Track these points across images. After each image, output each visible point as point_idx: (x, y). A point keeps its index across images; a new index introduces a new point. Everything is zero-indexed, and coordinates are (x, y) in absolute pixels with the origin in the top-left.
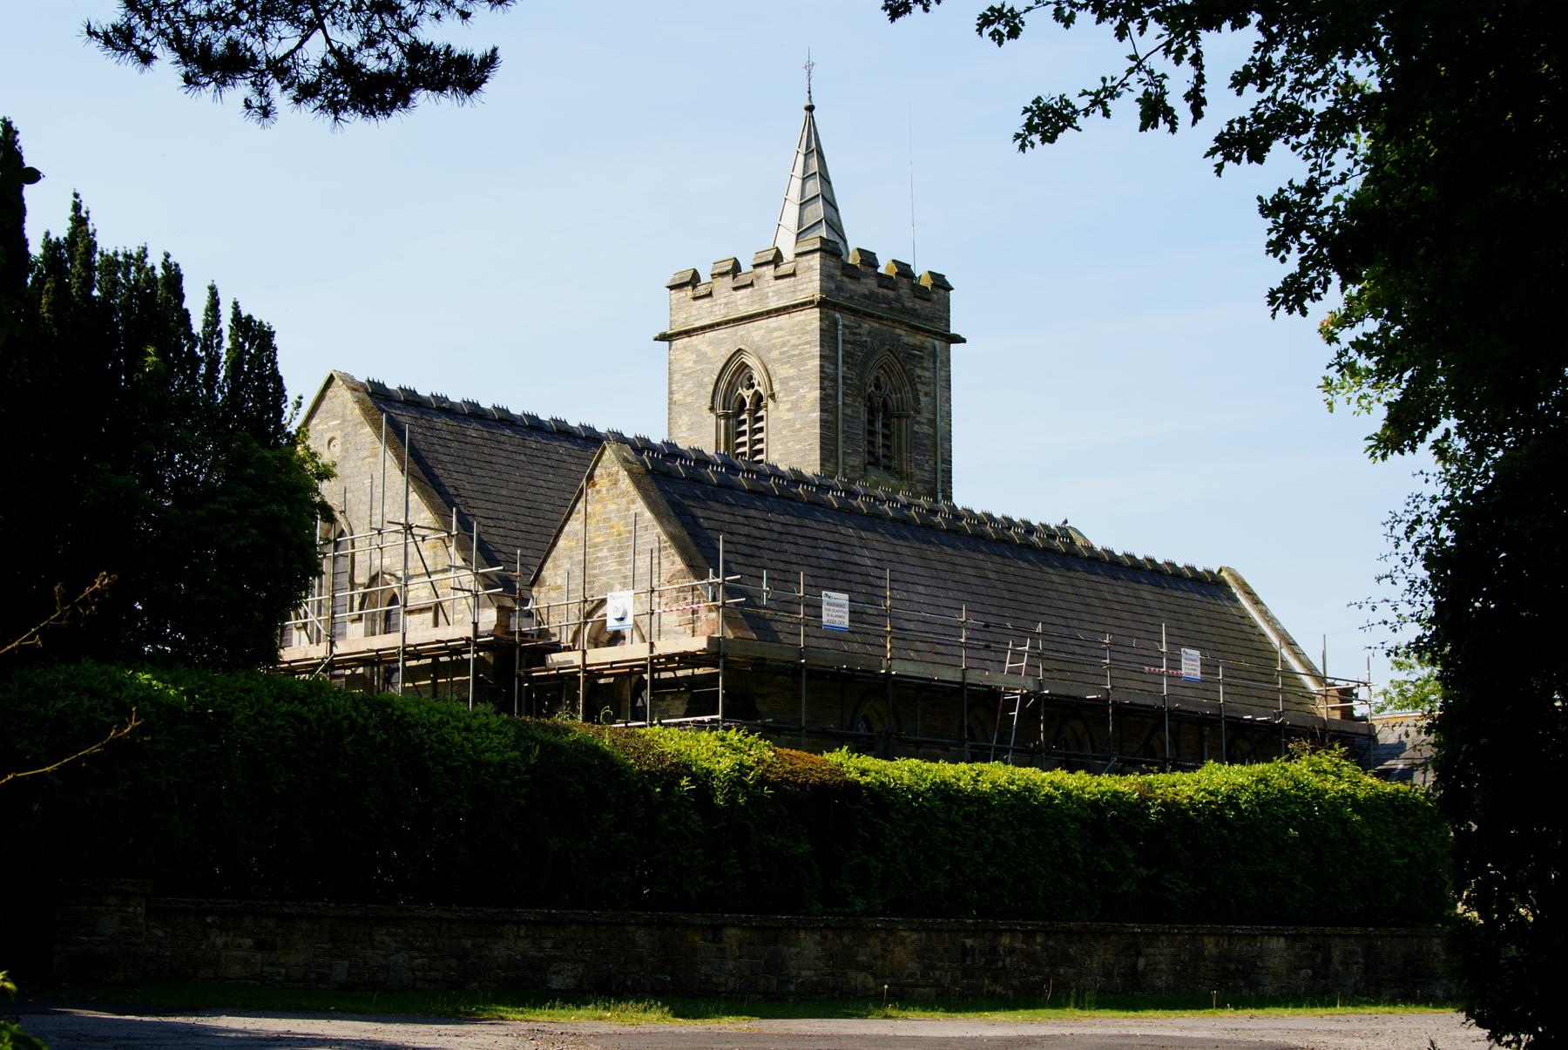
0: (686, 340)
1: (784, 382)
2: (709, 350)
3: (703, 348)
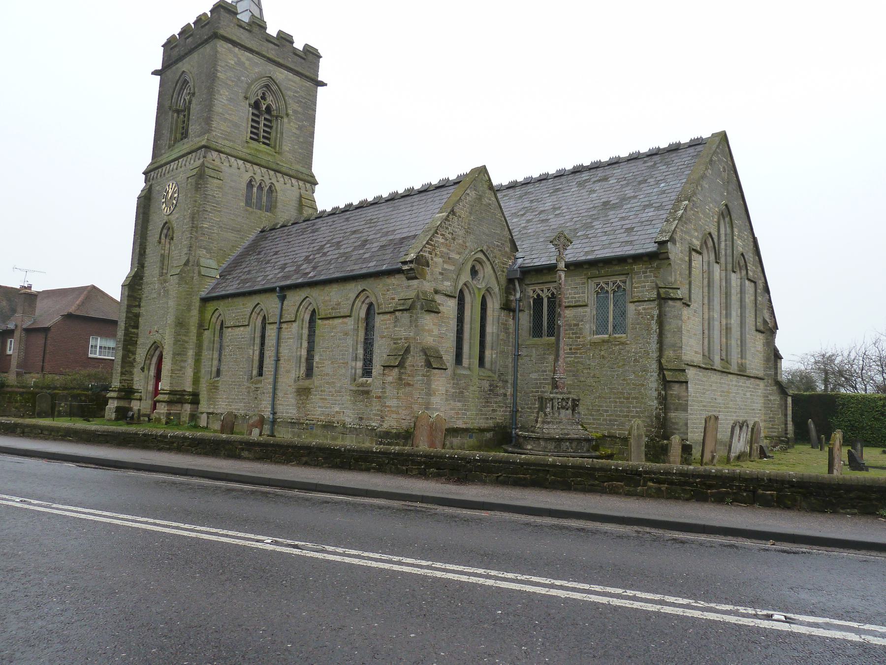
1: (295, 112)
2: (247, 63)
3: (243, 59)
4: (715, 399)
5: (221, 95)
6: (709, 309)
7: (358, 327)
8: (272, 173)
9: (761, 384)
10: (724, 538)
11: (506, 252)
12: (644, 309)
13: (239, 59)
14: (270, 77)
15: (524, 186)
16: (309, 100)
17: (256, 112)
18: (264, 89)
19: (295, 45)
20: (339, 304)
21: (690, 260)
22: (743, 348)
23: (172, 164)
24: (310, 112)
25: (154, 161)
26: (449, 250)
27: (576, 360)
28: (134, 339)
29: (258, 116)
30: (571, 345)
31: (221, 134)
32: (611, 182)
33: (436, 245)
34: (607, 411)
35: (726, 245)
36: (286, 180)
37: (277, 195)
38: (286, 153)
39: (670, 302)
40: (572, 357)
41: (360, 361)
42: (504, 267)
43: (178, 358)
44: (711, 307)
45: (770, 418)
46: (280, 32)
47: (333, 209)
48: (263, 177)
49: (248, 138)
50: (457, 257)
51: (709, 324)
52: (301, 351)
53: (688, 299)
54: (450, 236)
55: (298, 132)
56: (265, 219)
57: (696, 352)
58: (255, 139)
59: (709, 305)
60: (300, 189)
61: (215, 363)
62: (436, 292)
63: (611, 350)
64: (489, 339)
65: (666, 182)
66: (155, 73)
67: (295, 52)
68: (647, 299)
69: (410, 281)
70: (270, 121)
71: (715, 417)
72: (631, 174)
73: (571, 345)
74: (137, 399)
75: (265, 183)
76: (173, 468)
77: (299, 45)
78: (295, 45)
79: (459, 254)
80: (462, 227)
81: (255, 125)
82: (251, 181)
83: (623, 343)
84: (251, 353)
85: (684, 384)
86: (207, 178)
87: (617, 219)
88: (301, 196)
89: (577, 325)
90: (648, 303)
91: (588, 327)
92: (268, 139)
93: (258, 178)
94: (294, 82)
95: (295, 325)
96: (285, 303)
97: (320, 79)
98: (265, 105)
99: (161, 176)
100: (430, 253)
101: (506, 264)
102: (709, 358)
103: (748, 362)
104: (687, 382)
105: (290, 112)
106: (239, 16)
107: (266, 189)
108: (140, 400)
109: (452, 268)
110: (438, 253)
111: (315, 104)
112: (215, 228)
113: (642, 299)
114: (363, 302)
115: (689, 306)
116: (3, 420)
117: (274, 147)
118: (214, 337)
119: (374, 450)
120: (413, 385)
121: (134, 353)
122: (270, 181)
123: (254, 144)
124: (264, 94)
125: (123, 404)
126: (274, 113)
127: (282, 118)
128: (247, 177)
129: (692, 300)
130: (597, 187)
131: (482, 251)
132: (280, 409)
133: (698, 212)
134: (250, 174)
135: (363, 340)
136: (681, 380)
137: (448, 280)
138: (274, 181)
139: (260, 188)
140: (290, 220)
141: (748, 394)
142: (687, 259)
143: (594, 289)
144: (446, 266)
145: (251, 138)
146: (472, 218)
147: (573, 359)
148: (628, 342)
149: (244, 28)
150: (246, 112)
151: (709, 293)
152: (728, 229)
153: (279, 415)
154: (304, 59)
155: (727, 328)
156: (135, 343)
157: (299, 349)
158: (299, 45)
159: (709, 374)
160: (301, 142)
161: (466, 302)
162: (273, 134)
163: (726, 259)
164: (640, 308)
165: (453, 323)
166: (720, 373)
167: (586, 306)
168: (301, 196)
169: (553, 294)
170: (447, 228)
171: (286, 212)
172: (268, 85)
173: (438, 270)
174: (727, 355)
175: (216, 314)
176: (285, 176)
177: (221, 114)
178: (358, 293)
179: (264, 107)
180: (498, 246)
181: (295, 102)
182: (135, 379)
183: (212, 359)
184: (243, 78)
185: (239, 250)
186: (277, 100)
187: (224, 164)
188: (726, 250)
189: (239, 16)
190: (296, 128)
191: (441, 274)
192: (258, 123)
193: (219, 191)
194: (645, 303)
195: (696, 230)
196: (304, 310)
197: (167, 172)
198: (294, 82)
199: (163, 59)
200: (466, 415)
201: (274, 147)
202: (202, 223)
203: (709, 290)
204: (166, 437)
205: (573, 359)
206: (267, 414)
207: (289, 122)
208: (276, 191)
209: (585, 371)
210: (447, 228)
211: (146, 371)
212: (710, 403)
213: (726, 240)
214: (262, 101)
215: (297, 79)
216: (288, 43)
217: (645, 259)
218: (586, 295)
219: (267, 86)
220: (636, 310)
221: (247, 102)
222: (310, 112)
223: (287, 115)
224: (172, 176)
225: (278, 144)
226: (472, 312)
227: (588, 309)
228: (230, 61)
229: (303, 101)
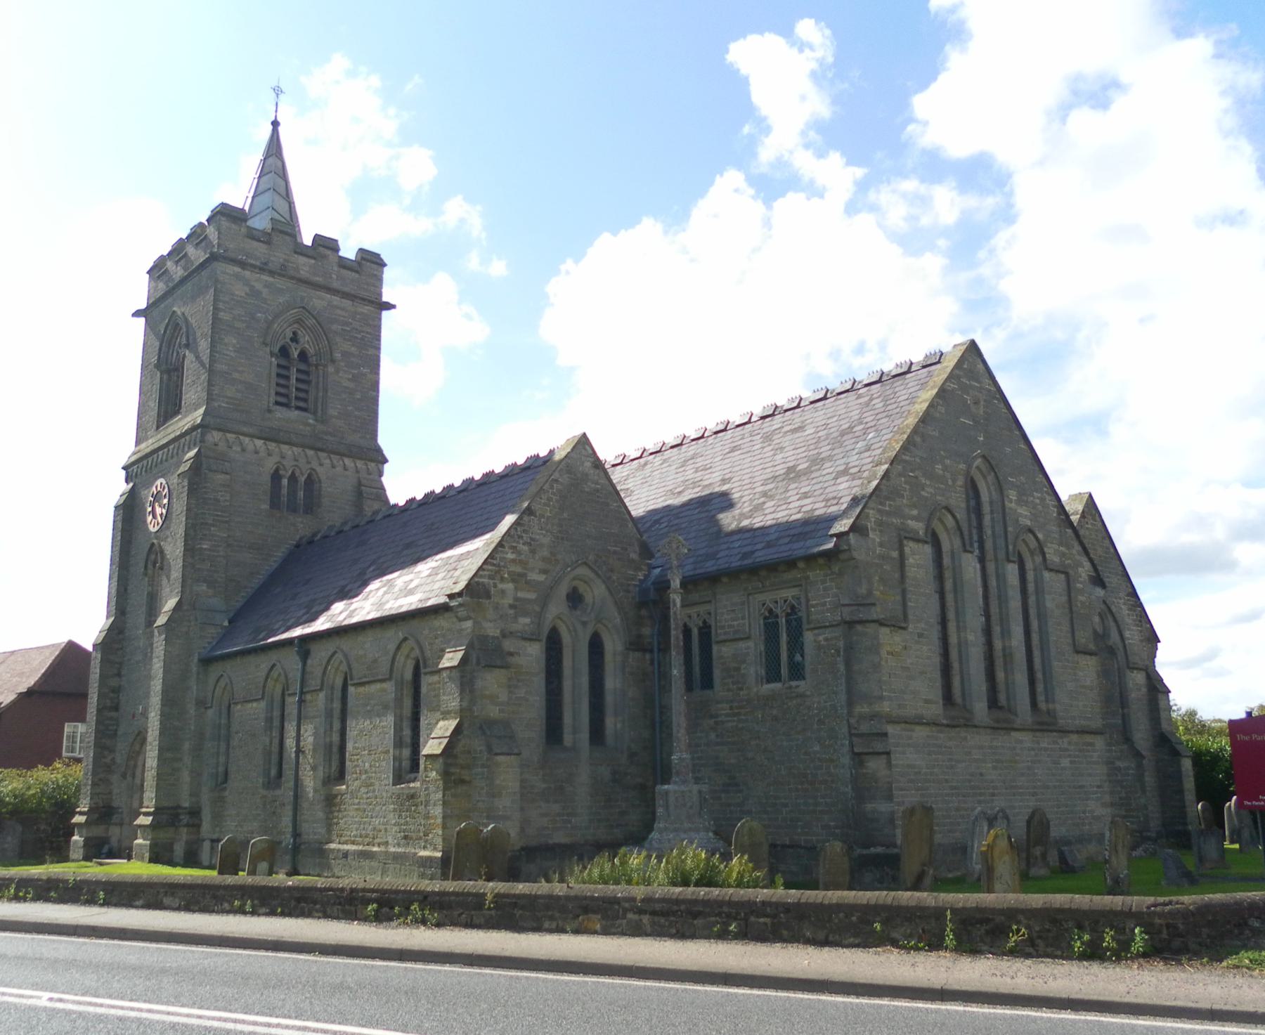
2: (265, 291)
3: (258, 286)
4: (981, 774)
5: (226, 345)
6: (958, 628)
7: (402, 694)
8: (310, 453)
9: (1099, 742)
10: (1237, 1027)
11: (633, 561)
12: (826, 639)
13: (252, 288)
14: (304, 308)
15: (694, 442)
16: (367, 333)
17: (283, 362)
18: (295, 326)
19: (341, 253)
20: (375, 661)
21: (902, 556)
22: (406, 752)
23: (160, 453)
24: (371, 352)
25: (138, 448)
26: (526, 569)
27: (740, 725)
28: (111, 728)
29: (287, 368)
30: (732, 701)
31: (227, 403)
32: (807, 433)
33: (502, 564)
34: (786, 805)
35: (993, 519)
36: (335, 462)
37: (320, 487)
38: (334, 420)
39: (859, 628)
40: (734, 721)
41: (406, 747)
42: (629, 585)
43: (169, 755)
44: (961, 624)
45: (1121, 798)
46: (317, 238)
47: (426, 496)
48: (297, 461)
49: (271, 405)
50: (542, 578)
51: (960, 652)
52: (331, 736)
53: (902, 617)
54: (526, 548)
55: (351, 385)
56: (301, 527)
57: (927, 701)
58: (283, 402)
59: (958, 621)
60: (358, 472)
61: (222, 759)
62: (504, 635)
63: (785, 706)
64: (609, 699)
65: (876, 431)
66: (137, 314)
67: (343, 263)
68: (827, 624)
69: (462, 623)
70: (307, 373)
71: (924, 807)
72: (835, 419)
73: (732, 701)
74: (116, 824)
75: (300, 469)
76: (298, 943)
77: (348, 251)
78: (341, 253)
79: (544, 572)
80: (547, 531)
81: (282, 381)
82: (277, 470)
83: (802, 696)
84: (268, 740)
85: (885, 756)
86: (205, 474)
87: (798, 497)
88: (360, 484)
89: (738, 669)
90: (830, 629)
91: (753, 670)
92: (305, 400)
93: (288, 463)
94: (343, 309)
95: (322, 695)
96: (309, 662)
97: (385, 299)
98: (298, 351)
99: (146, 471)
100: (490, 577)
101: (633, 579)
102: (965, 706)
103: (1058, 707)
104: (888, 753)
105: (338, 355)
106: (250, 223)
107: (302, 479)
108: (121, 824)
109: (532, 596)
110: (506, 576)
111: (378, 338)
112: (221, 549)
113: (823, 625)
114: (408, 656)
115: (904, 628)
116: (1255, 895)
117: (315, 413)
118: (220, 718)
119: (319, 886)
120: (470, 782)
121: (112, 751)
122: (309, 466)
123: (280, 413)
124: (294, 333)
125: (98, 831)
126: (313, 360)
127: (325, 366)
128: (270, 465)
129: (910, 617)
130: (786, 441)
131: (585, 564)
132: (305, 828)
133: (916, 477)
134: (275, 459)
135: (409, 715)
136: (876, 750)
137: (525, 614)
138: (315, 465)
139: (293, 478)
140: (335, 526)
141: (1065, 762)
142: (895, 554)
143: (760, 611)
144: (520, 595)
145: (277, 403)
146: (565, 515)
147: (735, 724)
148: (808, 693)
149: (259, 241)
150: (267, 363)
151: (956, 602)
152: (994, 493)
153: (305, 837)
154: (357, 272)
155: (1004, 656)
156: (114, 735)
157: (328, 733)
158: (348, 251)
159: (963, 734)
160: (358, 399)
161: (564, 645)
162: (311, 397)
163: (994, 543)
164: (821, 638)
165: (539, 682)
166: (989, 731)
167: (748, 638)
168: (360, 484)
169: (705, 622)
170: (520, 537)
171: (334, 512)
172: (300, 319)
173: (508, 600)
174: (1008, 699)
175: (222, 683)
176: (332, 456)
177: (227, 373)
178: (398, 642)
179: (296, 355)
180: (615, 552)
181: (345, 339)
182: (115, 791)
183: (218, 753)
184: (259, 315)
185: (256, 583)
186: (316, 340)
187: (234, 448)
188: (993, 527)
189: (250, 223)
190: (349, 380)
191: (511, 606)
192: (287, 378)
193: (225, 491)
194: (828, 630)
195: (914, 506)
196: (333, 671)
197: (154, 464)
198: (343, 309)
199: (149, 291)
200: (570, 822)
201: (315, 413)
202: (200, 544)
203: (956, 597)
204: (633, 899)
205: (735, 724)
206: (288, 839)
207: (337, 371)
208: (320, 481)
209: (753, 743)
210: (520, 537)
211: (129, 778)
212: (970, 781)
213: (992, 512)
214: (293, 345)
215: (347, 303)
216: (328, 252)
217: (821, 561)
218: (747, 621)
219: (299, 322)
220: (815, 641)
221: (268, 349)
222: (371, 352)
223: (333, 361)
224: (160, 472)
225: (320, 408)
226: (573, 661)
227: (751, 644)
228: (237, 293)
229: (359, 336)
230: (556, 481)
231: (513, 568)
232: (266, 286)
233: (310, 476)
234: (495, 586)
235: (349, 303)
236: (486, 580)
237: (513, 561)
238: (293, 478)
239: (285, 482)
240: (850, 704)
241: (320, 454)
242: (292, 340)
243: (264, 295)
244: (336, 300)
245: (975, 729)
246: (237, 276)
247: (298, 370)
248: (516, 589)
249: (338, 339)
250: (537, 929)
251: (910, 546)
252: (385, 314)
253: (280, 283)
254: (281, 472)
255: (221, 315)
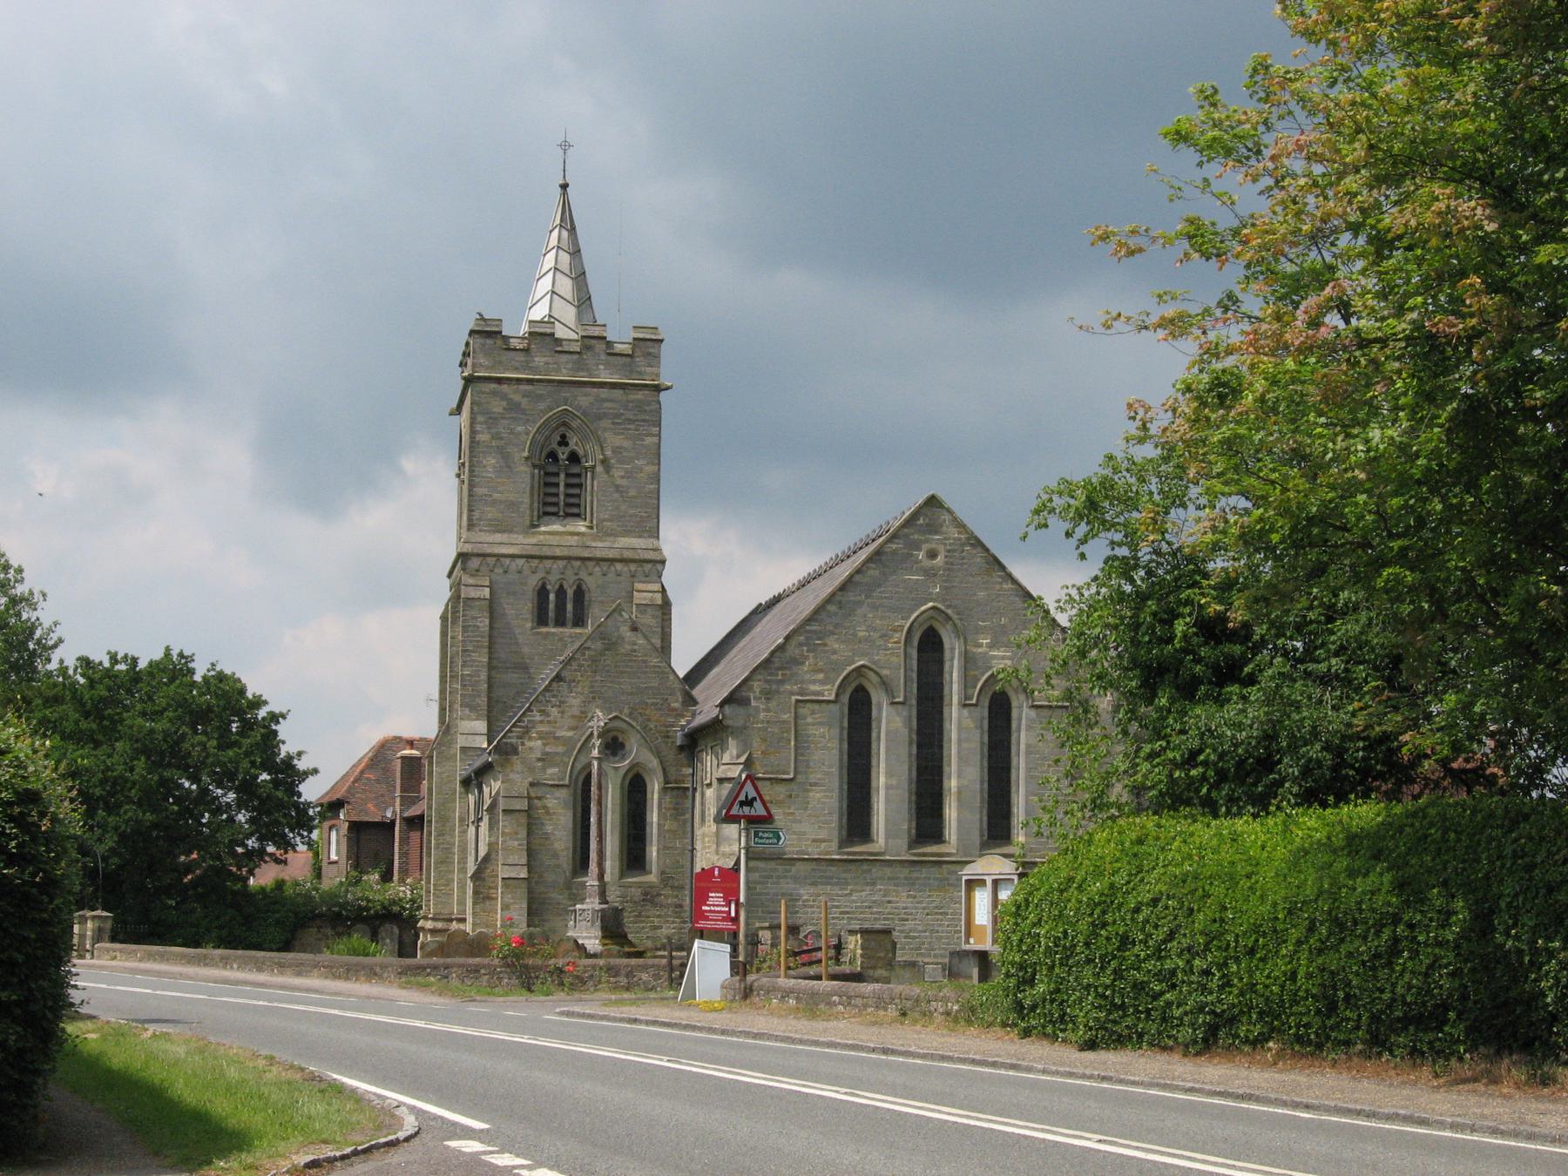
0: (493, 386)
2: (524, 402)
3: (517, 398)
11: (674, 710)
13: (510, 401)
128: (533, 581)
134: (540, 575)
138: (583, 575)
139: (561, 592)
191: (539, 760)
230: (589, 648)
231: (541, 728)
232: (524, 396)
233: (579, 587)
234: (523, 744)
235: (621, 392)
236: (514, 741)
237: (541, 722)
238: (561, 592)
239: (552, 597)
240: (718, 845)
241: (588, 563)
242: (560, 444)
243: (523, 406)
244: (604, 393)
245: (935, 872)
246: (494, 393)
247: (568, 475)
248: (544, 745)
249: (607, 435)
250: (305, 951)
251: (810, 716)
252: (663, 394)
253: (540, 390)
254: (549, 587)
255: (480, 437)
